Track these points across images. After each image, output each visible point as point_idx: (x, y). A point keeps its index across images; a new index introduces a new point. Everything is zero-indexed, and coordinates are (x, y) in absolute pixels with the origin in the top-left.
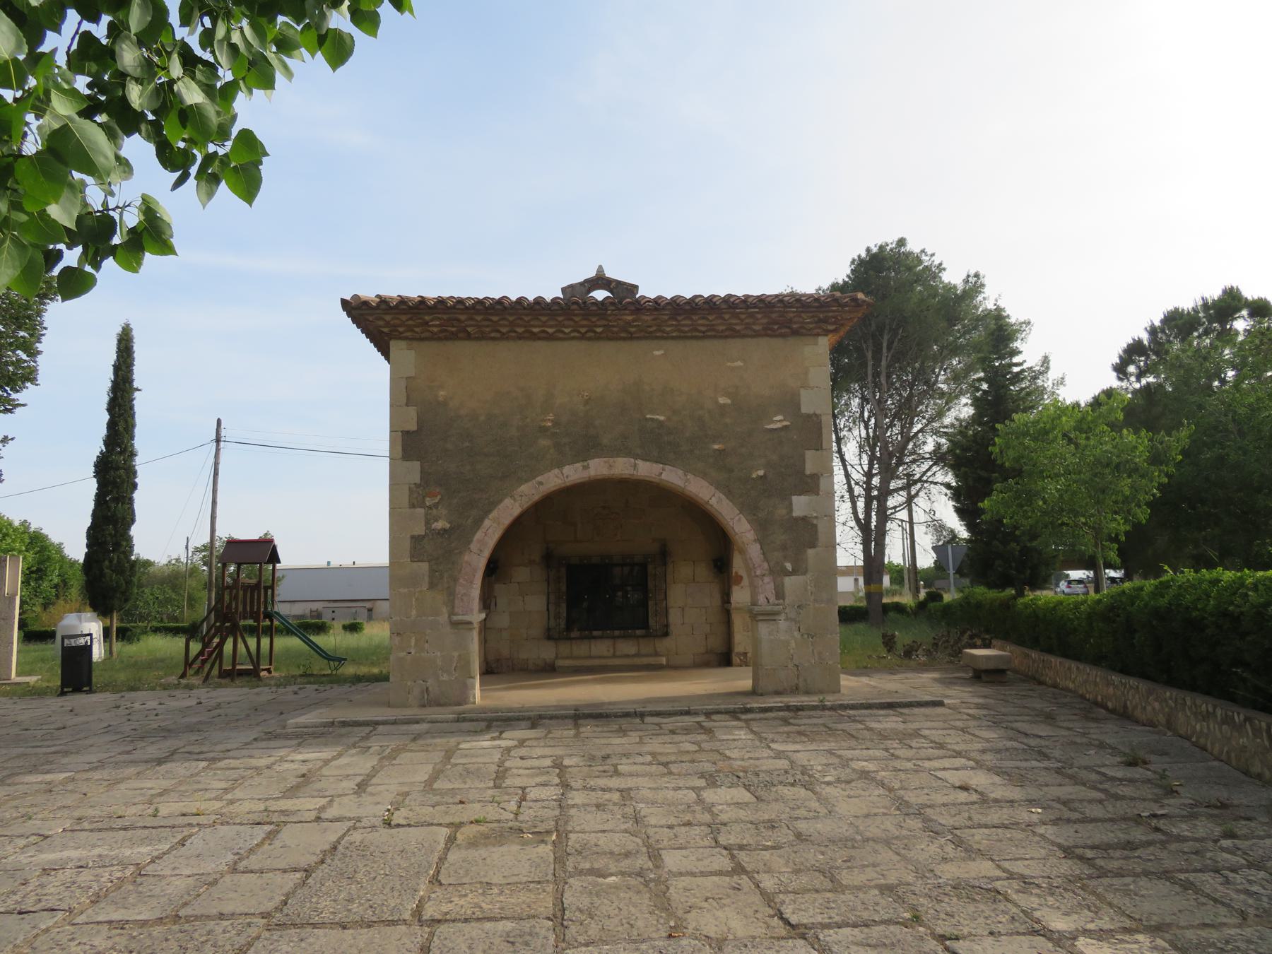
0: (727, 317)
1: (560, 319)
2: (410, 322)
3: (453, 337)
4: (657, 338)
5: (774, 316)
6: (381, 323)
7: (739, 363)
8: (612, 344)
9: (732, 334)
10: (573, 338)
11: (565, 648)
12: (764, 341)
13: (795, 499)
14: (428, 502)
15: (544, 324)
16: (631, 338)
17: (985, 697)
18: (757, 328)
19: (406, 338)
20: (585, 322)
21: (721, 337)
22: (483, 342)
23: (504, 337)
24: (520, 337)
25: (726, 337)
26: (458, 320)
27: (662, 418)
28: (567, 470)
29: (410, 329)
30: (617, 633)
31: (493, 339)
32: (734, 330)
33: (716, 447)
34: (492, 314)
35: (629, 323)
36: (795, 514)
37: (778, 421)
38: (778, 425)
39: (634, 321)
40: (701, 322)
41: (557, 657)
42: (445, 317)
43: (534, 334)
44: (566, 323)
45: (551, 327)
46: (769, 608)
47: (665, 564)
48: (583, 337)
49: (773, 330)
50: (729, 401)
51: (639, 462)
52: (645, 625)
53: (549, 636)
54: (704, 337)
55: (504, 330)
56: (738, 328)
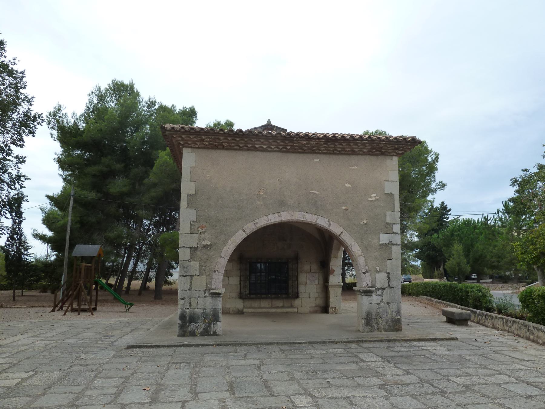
0: (352, 144)
1: (270, 141)
2: (195, 139)
3: (215, 148)
4: (316, 153)
5: (374, 145)
6: (180, 139)
7: (356, 167)
8: (294, 155)
9: (353, 153)
10: (275, 151)
11: (248, 303)
12: (367, 157)
13: (382, 235)
15: (262, 143)
16: (304, 152)
18: (365, 150)
19: (191, 147)
20: (283, 144)
21: (331, 154)
22: (230, 151)
23: (241, 149)
24: (249, 149)
25: (349, 154)
26: (219, 139)
27: (318, 193)
28: (270, 217)
29: (194, 143)
30: (273, 296)
31: (236, 150)
32: (354, 151)
33: (344, 208)
34: (236, 137)
35: (304, 145)
37: (374, 196)
38: (374, 199)
39: (307, 144)
40: (339, 146)
41: (244, 307)
42: (213, 137)
43: (256, 148)
44: (273, 143)
45: (265, 145)
46: (368, 289)
47: (297, 263)
48: (280, 151)
49: (373, 152)
50: (350, 186)
51: (306, 214)
52: (287, 293)
53: (241, 297)
54: (340, 154)
55: (241, 145)
56: (356, 150)
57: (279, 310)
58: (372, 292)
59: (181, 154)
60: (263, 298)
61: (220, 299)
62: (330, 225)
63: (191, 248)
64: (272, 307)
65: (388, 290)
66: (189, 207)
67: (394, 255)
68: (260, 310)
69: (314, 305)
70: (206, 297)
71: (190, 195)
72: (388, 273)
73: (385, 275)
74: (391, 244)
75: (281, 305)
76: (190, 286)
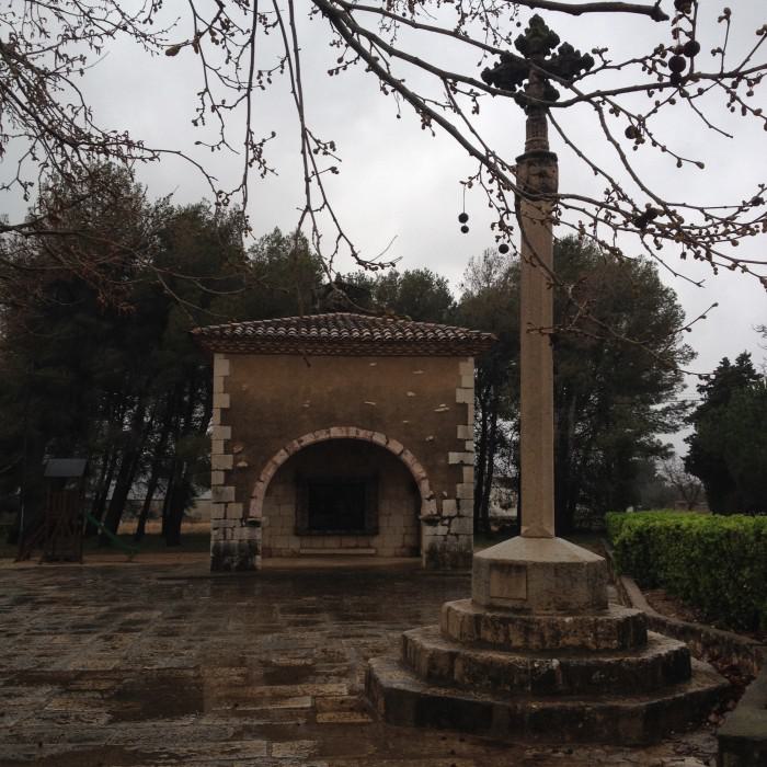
11: (306, 542)
13: (451, 454)
14: (236, 450)
16: (357, 355)
17: (52, 576)
35: (355, 348)
36: (450, 463)
37: (443, 407)
53: (298, 533)
57: (351, 551)
58: (438, 521)
59: (213, 359)
60: (329, 535)
61: (260, 529)
62: (387, 443)
63: (225, 471)
64: (340, 548)
65: (457, 520)
66: (223, 423)
67: (465, 477)
68: (323, 552)
69: (400, 545)
70: (242, 526)
71: (223, 411)
72: (458, 500)
73: (453, 502)
74: (462, 464)
75: (353, 544)
76: (225, 514)
